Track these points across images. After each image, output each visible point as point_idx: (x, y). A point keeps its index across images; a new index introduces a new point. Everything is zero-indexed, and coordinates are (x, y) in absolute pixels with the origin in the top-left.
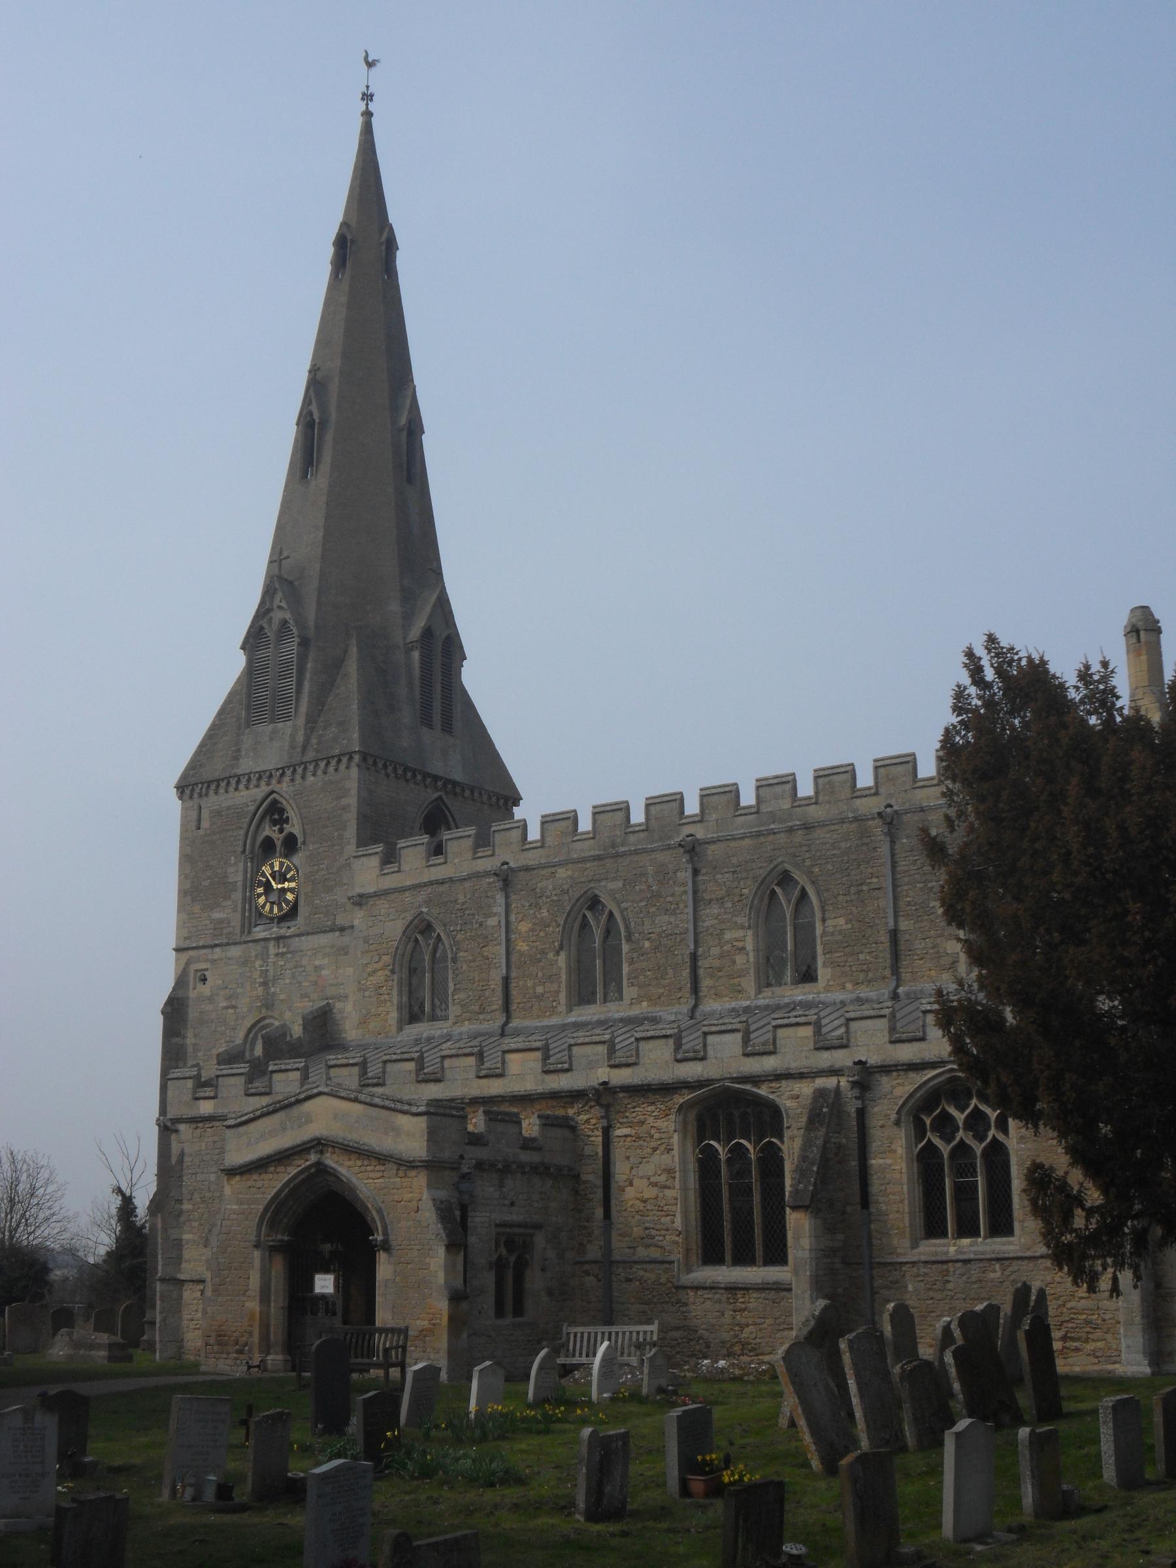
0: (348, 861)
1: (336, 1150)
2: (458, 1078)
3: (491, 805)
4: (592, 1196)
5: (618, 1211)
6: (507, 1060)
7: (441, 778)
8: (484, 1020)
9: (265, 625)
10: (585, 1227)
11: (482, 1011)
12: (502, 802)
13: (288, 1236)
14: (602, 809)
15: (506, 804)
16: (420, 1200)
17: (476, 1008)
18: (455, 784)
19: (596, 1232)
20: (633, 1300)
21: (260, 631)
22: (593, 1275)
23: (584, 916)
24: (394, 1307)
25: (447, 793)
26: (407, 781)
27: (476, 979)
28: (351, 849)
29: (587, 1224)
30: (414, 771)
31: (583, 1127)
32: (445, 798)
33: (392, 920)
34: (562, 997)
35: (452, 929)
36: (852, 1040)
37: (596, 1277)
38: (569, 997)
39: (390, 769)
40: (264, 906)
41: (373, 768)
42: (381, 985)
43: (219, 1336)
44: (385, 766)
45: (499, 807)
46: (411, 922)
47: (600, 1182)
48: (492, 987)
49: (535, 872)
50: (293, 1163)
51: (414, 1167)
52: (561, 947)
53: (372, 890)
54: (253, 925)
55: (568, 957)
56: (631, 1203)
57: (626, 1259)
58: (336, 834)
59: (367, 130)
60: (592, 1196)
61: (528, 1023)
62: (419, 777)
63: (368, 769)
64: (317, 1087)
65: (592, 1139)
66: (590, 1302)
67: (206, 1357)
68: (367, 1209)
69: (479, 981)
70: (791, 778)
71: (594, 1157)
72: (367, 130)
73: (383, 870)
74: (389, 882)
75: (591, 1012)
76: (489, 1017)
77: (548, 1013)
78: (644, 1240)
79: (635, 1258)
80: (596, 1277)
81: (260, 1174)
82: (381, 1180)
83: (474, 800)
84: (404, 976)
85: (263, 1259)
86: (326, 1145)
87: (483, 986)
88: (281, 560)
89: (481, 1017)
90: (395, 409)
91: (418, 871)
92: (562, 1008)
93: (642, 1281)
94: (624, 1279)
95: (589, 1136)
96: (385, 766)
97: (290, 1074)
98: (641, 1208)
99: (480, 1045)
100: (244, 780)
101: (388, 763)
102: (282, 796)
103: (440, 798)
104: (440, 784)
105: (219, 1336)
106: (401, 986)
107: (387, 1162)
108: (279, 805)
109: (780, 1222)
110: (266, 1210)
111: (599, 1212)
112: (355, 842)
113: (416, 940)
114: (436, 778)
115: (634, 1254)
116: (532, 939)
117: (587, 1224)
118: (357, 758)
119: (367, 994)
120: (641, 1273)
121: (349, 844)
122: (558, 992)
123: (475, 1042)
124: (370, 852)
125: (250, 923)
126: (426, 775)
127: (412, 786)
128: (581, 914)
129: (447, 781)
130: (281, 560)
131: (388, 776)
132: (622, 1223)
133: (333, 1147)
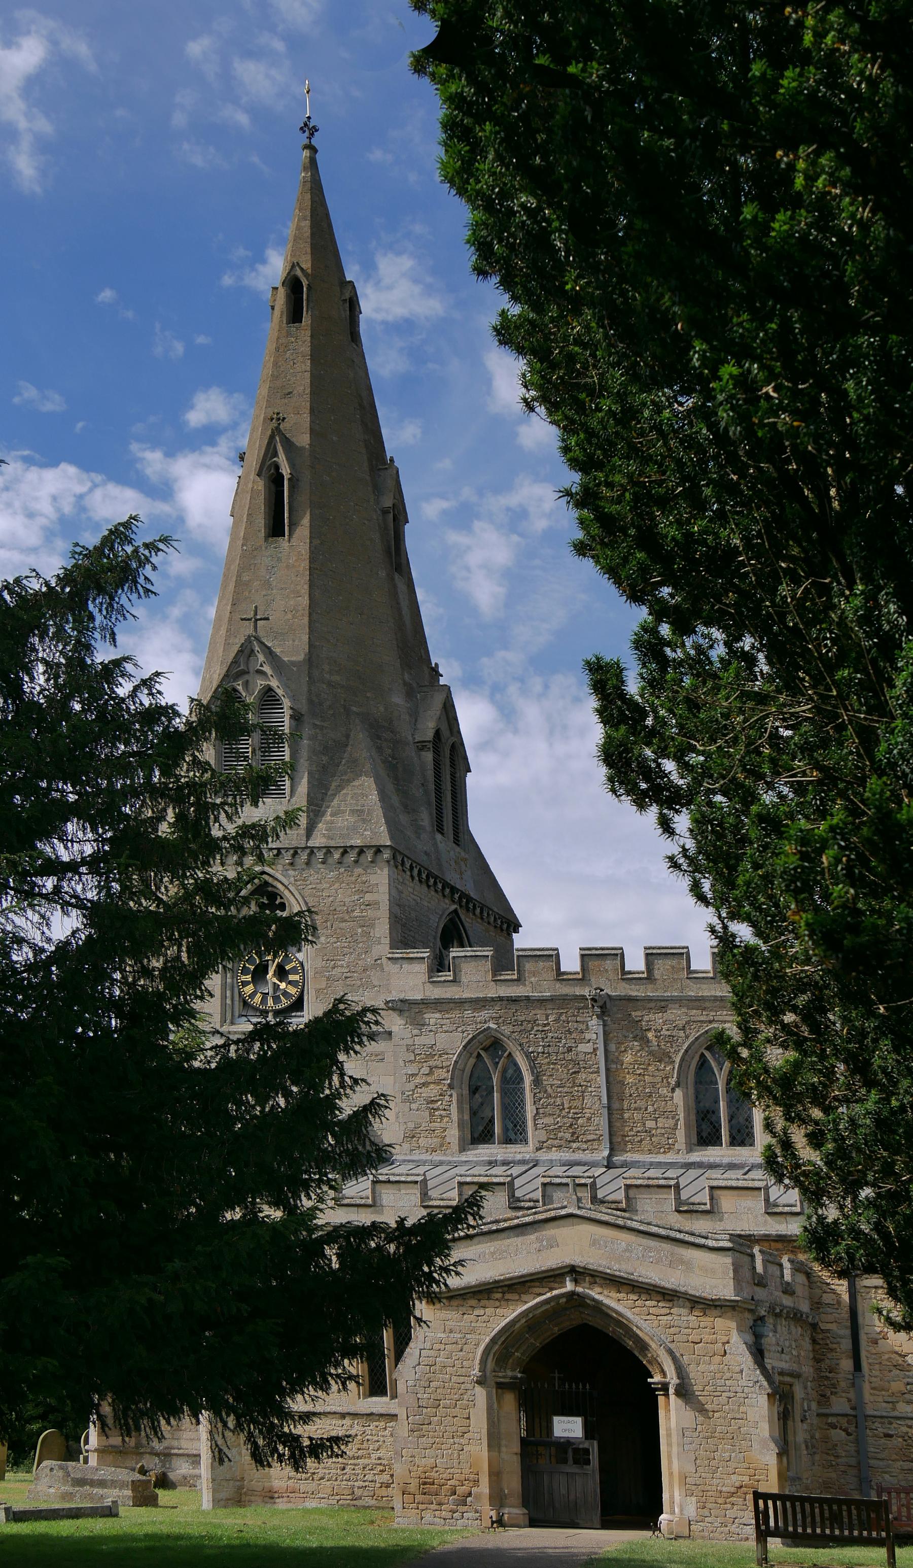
0: (379, 962)
1: (598, 1280)
2: (649, 1209)
3: (495, 927)
4: (834, 1346)
5: (870, 1364)
6: (715, 1196)
7: (458, 890)
8: (579, 1149)
9: (240, 688)
10: (827, 1378)
11: (575, 1138)
12: (505, 926)
13: (520, 1372)
14: (539, 953)
15: (508, 927)
16: (728, 1342)
17: (568, 1136)
18: (469, 899)
19: (843, 1384)
20: (894, 1457)
21: (267, 692)
22: (841, 1428)
23: (702, 1055)
24: (696, 1459)
25: (461, 906)
26: (429, 887)
27: (566, 1106)
28: (383, 948)
29: (830, 1375)
30: (436, 878)
31: (820, 1274)
32: (459, 911)
33: (446, 1032)
34: (681, 1134)
35: (530, 1050)
36: (379, 1201)
37: (845, 1430)
38: (688, 1136)
39: (416, 872)
40: (252, 996)
41: (400, 867)
42: (435, 1099)
43: (425, 1483)
44: (411, 868)
45: (502, 930)
46: (474, 1038)
47: (848, 1332)
48: (587, 1115)
49: (639, 1003)
50: (531, 1290)
51: (716, 1306)
52: (678, 1085)
53: (419, 997)
54: (237, 1014)
55: (685, 1096)
56: (887, 1356)
57: (885, 1414)
58: (360, 930)
59: (315, 188)
60: (834, 1346)
61: (636, 1157)
62: (440, 886)
63: (397, 867)
64: (565, 1207)
65: (833, 1287)
66: (837, 1457)
67: (404, 1508)
68: (644, 1347)
69: (570, 1108)
70: (620, 951)
71: (836, 1306)
72: (315, 188)
73: (432, 977)
74: (436, 993)
75: (513, 1150)
76: (585, 1146)
77: (662, 1150)
78: (905, 1396)
79: (896, 1414)
80: (844, 1430)
81: (479, 1300)
82: (669, 1318)
83: (482, 919)
84: (690, 1093)
85: (489, 1397)
86: (583, 1273)
87: (575, 1113)
88: (257, 620)
89: (574, 1145)
90: (377, 489)
91: (481, 984)
92: (455, 1147)
93: (906, 1438)
94: (882, 1435)
95: (828, 1284)
96: (411, 868)
97: (404, 1190)
98: (900, 1362)
99: (424, 1175)
100: (320, 855)
101: (414, 865)
102: (277, 879)
103: (455, 911)
104: (456, 896)
105: (425, 1483)
106: (462, 1103)
107: (675, 1298)
108: (270, 889)
109: (380, 1367)
110: (493, 1341)
111: (847, 1364)
112: (388, 942)
113: (479, 1055)
114: (453, 890)
115: (894, 1409)
116: (638, 1072)
117: (830, 1375)
118: (387, 855)
119: (414, 1106)
120: (905, 1429)
121: (380, 943)
122: (675, 1127)
123: (421, 1170)
124: (411, 955)
125: (233, 1015)
126: (446, 885)
127: (433, 893)
128: (700, 1053)
129: (463, 895)
130: (257, 620)
131: (412, 877)
132: (875, 1377)
133: (592, 1276)
